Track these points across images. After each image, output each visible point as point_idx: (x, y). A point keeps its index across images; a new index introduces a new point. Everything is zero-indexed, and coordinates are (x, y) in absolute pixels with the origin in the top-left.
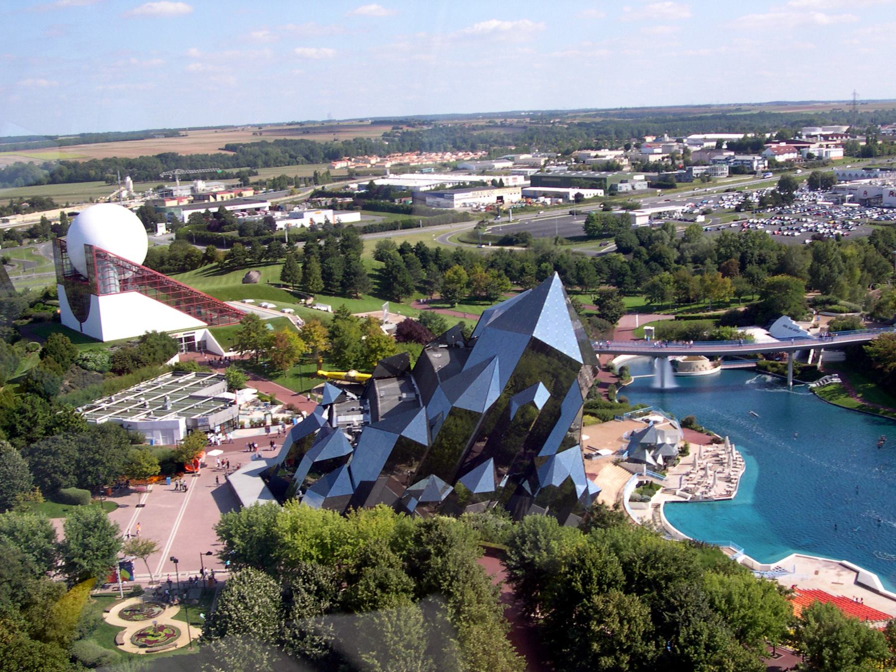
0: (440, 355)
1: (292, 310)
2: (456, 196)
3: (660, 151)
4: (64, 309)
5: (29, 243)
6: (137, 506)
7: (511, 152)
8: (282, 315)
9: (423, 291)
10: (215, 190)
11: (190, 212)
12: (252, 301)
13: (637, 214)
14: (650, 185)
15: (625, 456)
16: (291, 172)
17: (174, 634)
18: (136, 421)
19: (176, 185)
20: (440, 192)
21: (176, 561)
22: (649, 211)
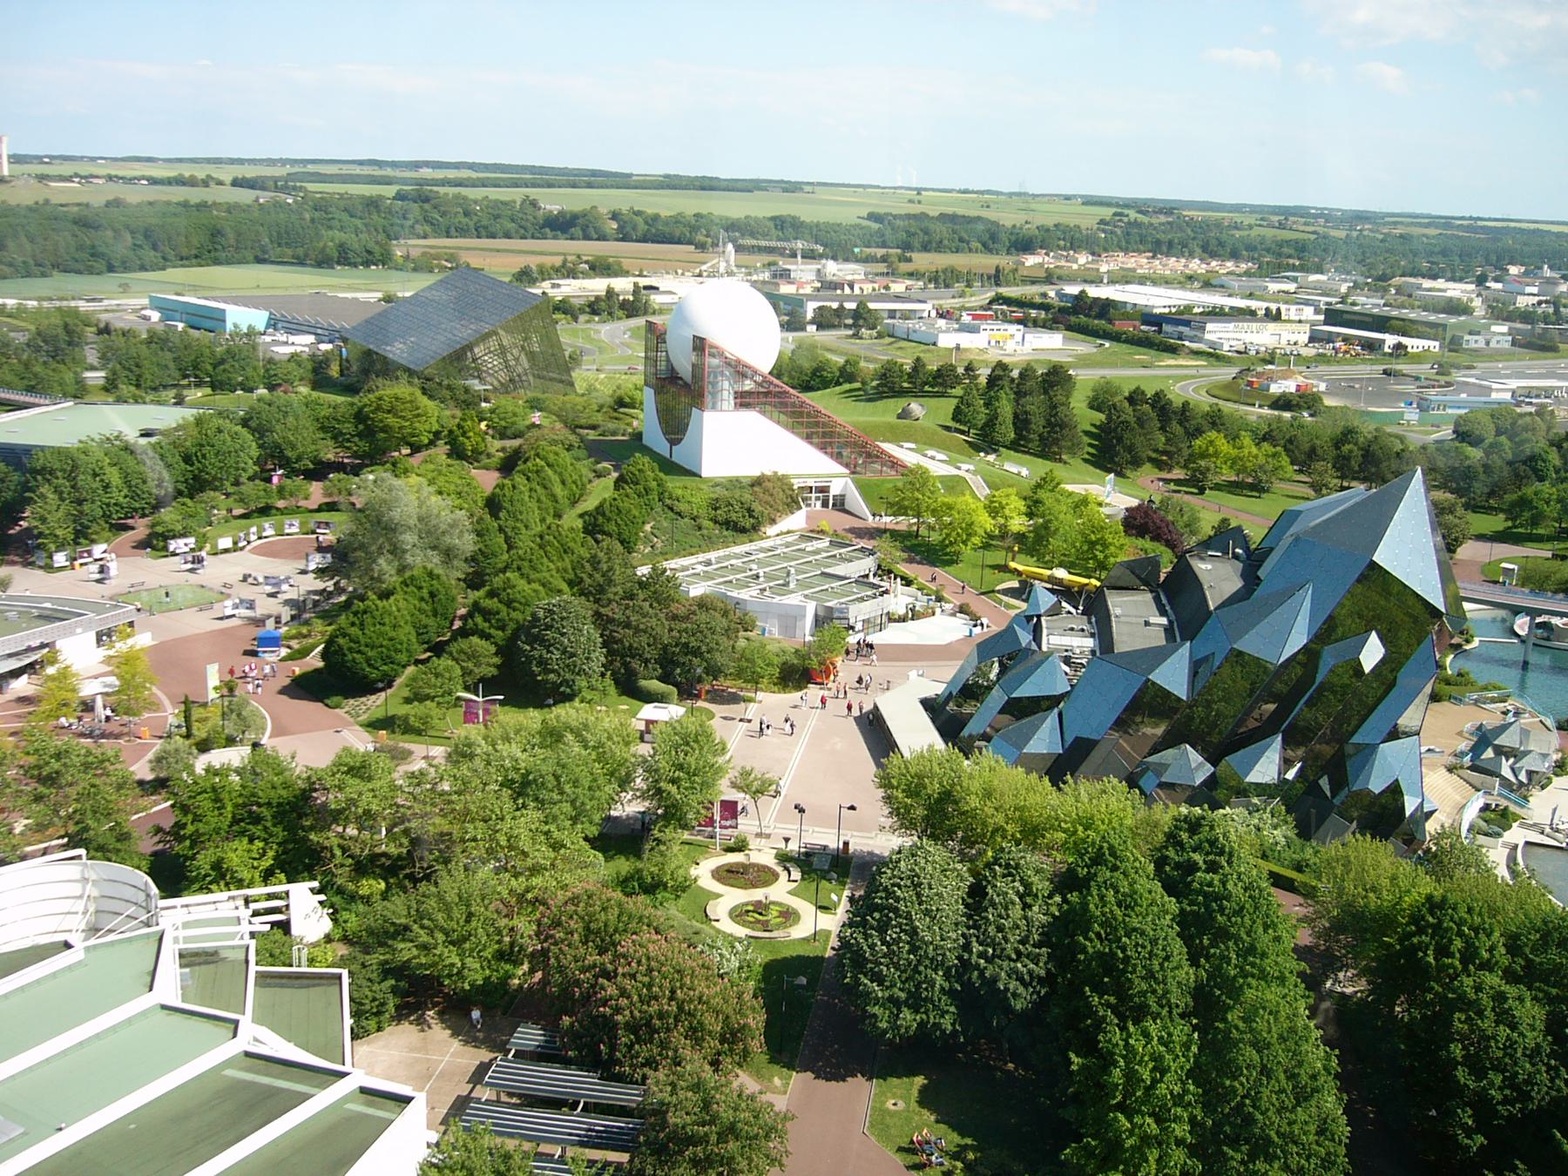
0: (1209, 567)
1: (972, 467)
2: (1209, 326)
3: (1535, 290)
4: (646, 420)
5: (588, 322)
6: (741, 720)
7: (1294, 268)
8: (955, 472)
9: (1159, 465)
10: (849, 278)
11: (815, 305)
12: (913, 446)
13: (1495, 386)
14: (1514, 343)
15: (1467, 760)
16: (960, 261)
17: (789, 916)
18: (746, 597)
19: (797, 263)
20: (1182, 318)
21: (802, 811)
22: (1514, 384)
